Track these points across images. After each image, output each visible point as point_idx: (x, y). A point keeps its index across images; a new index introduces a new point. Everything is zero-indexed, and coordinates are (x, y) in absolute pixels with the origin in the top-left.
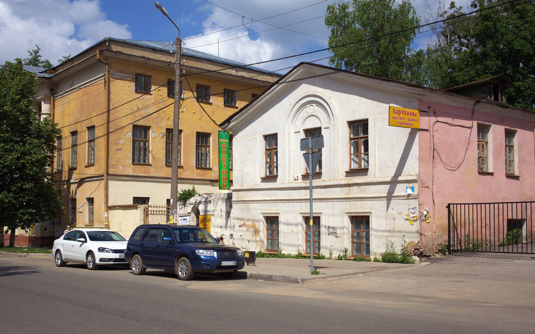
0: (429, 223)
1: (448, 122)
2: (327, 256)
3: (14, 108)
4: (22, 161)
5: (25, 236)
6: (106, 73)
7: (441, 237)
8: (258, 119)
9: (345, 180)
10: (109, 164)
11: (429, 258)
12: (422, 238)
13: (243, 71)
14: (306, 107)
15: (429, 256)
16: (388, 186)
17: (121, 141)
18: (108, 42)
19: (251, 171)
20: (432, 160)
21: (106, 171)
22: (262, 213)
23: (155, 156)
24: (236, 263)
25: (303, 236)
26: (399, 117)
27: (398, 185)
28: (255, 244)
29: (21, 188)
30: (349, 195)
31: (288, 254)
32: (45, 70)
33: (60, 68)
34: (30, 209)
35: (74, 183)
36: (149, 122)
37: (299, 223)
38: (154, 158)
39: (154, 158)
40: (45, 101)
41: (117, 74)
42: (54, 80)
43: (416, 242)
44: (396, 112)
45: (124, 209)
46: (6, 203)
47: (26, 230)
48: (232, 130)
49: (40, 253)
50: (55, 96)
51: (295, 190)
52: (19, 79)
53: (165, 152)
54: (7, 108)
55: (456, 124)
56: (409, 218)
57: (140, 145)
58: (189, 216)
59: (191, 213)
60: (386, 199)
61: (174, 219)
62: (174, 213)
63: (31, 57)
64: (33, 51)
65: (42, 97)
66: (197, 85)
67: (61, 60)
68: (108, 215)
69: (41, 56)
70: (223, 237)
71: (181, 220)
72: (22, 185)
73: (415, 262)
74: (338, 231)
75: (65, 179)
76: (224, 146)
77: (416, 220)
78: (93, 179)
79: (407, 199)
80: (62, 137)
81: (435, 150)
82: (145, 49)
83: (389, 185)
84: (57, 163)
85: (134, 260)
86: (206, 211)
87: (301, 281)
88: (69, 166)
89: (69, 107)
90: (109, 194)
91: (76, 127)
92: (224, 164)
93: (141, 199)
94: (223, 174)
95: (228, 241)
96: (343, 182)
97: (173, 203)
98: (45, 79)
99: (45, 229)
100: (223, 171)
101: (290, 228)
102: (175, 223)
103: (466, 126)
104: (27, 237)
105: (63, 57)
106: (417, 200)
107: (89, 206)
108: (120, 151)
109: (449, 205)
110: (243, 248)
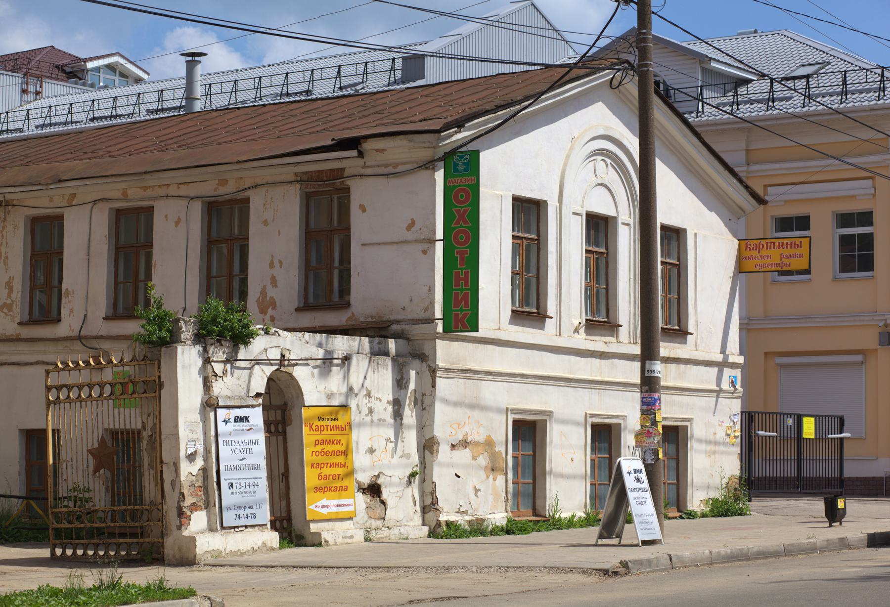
70: (379, 482)
94: (457, 285)
95: (399, 494)
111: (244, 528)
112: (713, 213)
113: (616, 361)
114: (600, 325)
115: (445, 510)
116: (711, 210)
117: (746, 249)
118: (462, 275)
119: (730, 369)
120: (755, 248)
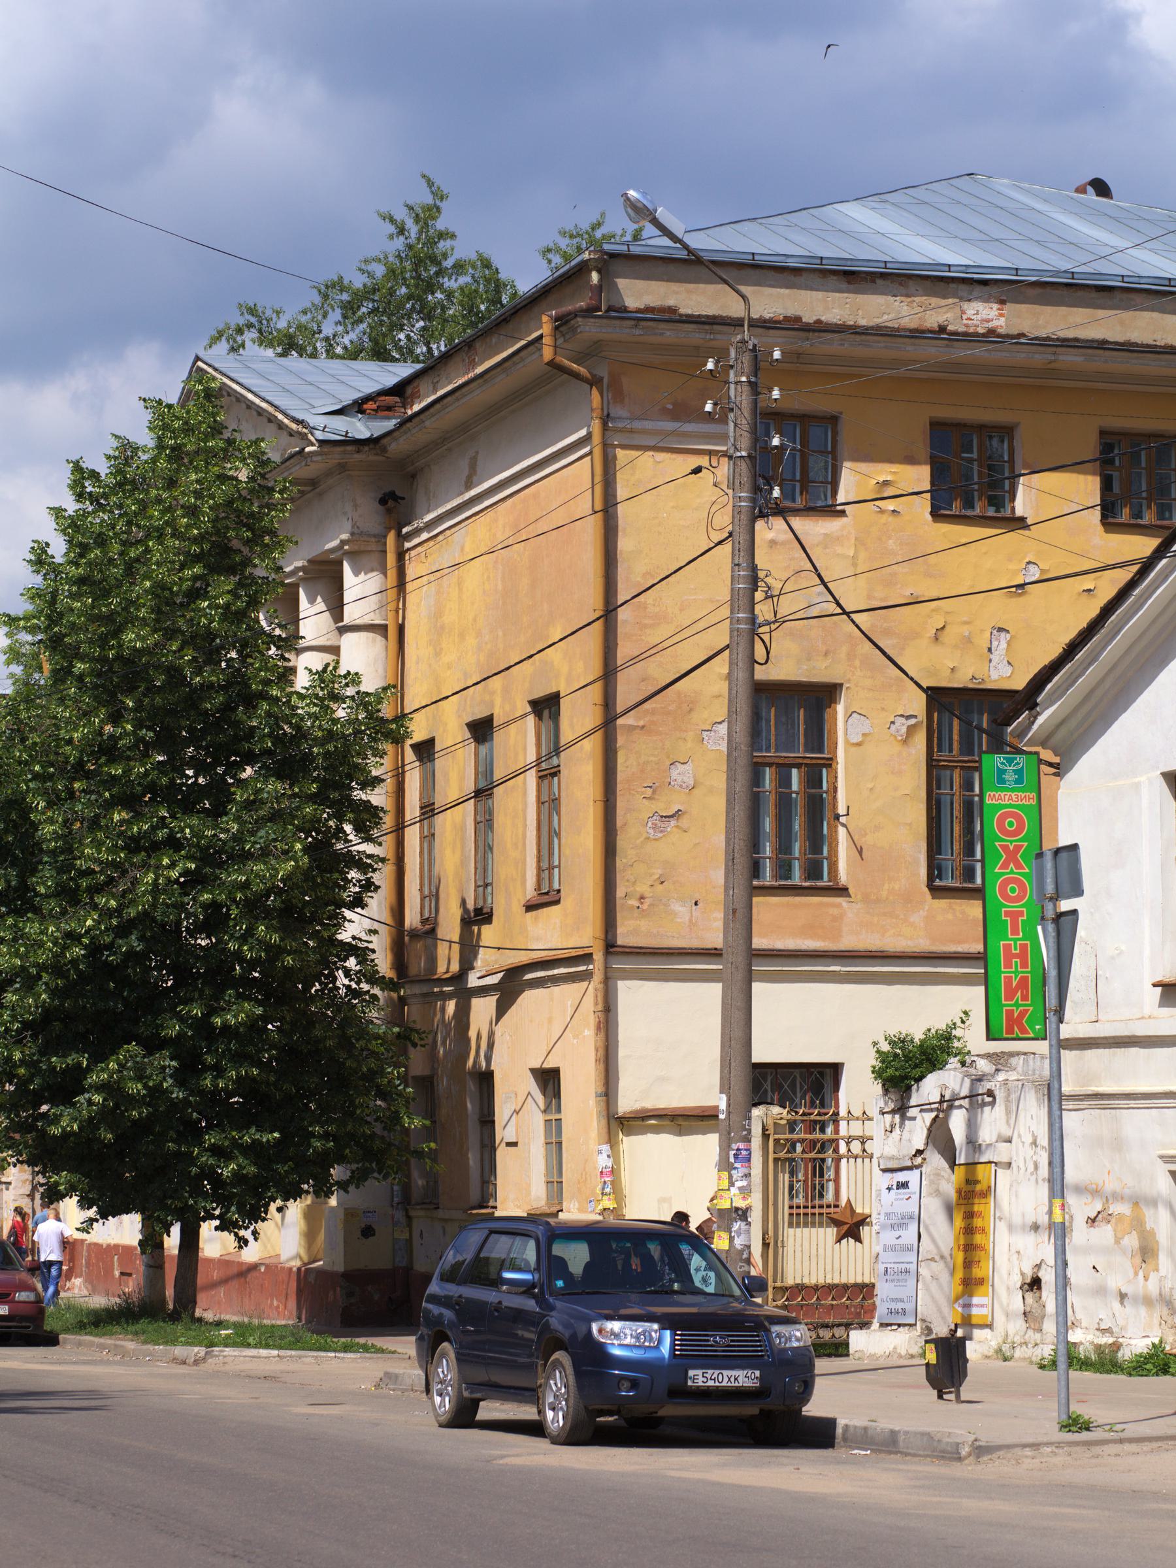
3: (171, 634)
4: (207, 896)
5: (283, 1268)
6: (596, 426)
8: (1142, 692)
10: (620, 892)
17: (682, 774)
18: (599, 271)
19: (1123, 948)
21: (600, 933)
23: (867, 841)
24: (761, 1379)
28: (1143, 1311)
29: (203, 1026)
32: (355, 402)
33: (424, 385)
34: (253, 1130)
35: (483, 991)
36: (829, 661)
38: (860, 852)
39: (860, 852)
40: (353, 555)
41: (648, 425)
42: (396, 448)
45: (680, 1132)
46: (132, 1101)
47: (242, 1233)
49: (267, 1346)
50: (405, 530)
52: (198, 481)
54: (138, 635)
57: (788, 784)
58: (917, 1167)
59: (926, 1155)
61: (734, 1190)
62: (732, 1160)
63: (399, 243)
64: (411, 208)
65: (343, 542)
66: (1103, 433)
67: (558, 250)
68: (617, 1161)
69: (453, 236)
71: (889, 1189)
72: (211, 1012)
75: (447, 972)
76: (1011, 824)
78: (556, 972)
80: (437, 748)
82: (801, 280)
84: (422, 885)
85: (437, 1367)
86: (972, 1142)
87: (970, 1454)
88: (464, 902)
89: (460, 590)
90: (622, 1052)
91: (487, 698)
93: (797, 1073)
94: (1008, 965)
97: (729, 1113)
98: (349, 448)
99: (368, 1232)
100: (1007, 948)
102: (737, 1209)
104: (290, 1269)
105: (563, 233)
107: (545, 1111)
108: (673, 822)
110: (1104, 1331)
111: (896, 1327)
115: (1084, 1325)
118: (1016, 949)
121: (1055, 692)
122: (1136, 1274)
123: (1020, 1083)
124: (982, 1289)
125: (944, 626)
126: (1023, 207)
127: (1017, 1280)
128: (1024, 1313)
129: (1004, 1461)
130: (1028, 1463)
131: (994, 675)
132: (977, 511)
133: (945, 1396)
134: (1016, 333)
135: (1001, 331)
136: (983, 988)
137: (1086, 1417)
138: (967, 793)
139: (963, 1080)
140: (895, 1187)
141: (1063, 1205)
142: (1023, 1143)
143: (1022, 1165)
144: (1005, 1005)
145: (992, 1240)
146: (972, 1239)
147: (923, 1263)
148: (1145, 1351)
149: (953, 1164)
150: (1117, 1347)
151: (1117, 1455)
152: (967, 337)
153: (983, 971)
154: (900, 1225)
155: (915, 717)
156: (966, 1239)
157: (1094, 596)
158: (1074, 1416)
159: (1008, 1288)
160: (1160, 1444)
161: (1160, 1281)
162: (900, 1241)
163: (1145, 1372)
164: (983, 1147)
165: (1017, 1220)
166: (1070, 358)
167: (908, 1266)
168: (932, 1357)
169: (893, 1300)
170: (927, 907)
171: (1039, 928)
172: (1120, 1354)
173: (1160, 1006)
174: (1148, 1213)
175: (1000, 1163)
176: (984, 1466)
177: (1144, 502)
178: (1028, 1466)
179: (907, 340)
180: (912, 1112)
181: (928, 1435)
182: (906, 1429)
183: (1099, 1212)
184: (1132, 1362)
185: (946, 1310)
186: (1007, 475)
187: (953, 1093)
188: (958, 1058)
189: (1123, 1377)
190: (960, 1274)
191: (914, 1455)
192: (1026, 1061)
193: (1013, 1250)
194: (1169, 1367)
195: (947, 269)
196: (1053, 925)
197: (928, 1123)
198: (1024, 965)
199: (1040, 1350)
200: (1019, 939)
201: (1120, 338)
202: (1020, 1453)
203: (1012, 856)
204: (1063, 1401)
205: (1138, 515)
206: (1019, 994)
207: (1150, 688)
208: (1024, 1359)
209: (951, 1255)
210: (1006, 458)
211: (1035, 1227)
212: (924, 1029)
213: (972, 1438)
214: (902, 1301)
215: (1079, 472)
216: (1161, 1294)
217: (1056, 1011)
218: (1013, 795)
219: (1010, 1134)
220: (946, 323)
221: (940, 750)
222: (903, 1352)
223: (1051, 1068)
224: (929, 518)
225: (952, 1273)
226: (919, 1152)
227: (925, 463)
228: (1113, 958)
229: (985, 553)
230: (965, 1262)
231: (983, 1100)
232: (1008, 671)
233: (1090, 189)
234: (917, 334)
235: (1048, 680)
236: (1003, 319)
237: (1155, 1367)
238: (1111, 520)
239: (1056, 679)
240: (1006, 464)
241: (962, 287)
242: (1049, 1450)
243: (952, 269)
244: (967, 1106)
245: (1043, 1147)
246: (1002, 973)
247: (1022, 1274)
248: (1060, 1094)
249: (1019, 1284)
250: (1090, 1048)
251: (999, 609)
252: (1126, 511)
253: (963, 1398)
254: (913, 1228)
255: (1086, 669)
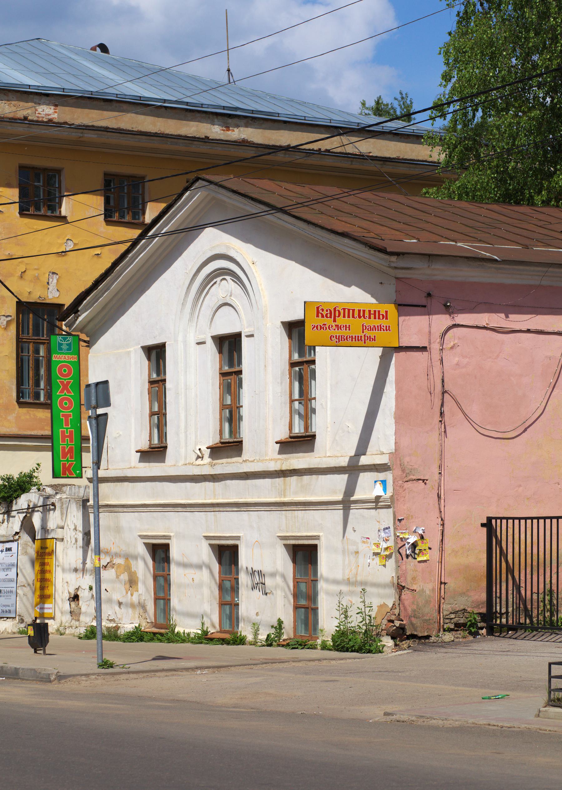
0: (425, 561)
1: (491, 325)
2: (250, 638)
7: (463, 594)
9: (276, 460)
11: (427, 641)
12: (403, 597)
13: (246, 126)
14: (215, 283)
15: (428, 637)
16: (345, 477)
19: (121, 433)
20: (437, 418)
22: (142, 537)
25: (212, 592)
26: (333, 324)
27: (362, 475)
28: (130, 611)
30: (285, 496)
31: (184, 633)
37: (203, 563)
43: (390, 606)
44: (324, 313)
48: (86, 330)
51: (196, 483)
53: (14, 368)
55: (517, 327)
56: (379, 551)
59: (21, 534)
60: (341, 506)
66: (106, 174)
71: (2, 551)
73: (385, 649)
74: (269, 581)
76: (65, 371)
77: (389, 557)
79: (376, 508)
81: (446, 395)
83: (347, 476)
86: (44, 528)
87: (55, 679)
92: (66, 417)
94: (63, 441)
96: (273, 467)
100: (63, 432)
101: (191, 573)
103: (550, 330)
106: (391, 510)
109: (489, 519)
110: (111, 621)
111: (6, 619)
112: (353, 287)
113: (228, 482)
114: (300, 441)
116: (349, 286)
117: (318, 316)
118: (67, 433)
119: (376, 473)
120: (329, 315)
121: (87, 305)
122: (127, 593)
123: (68, 500)
124: (49, 600)
125: (25, 271)
126: (66, 57)
127: (67, 596)
128: (70, 612)
129: (72, 682)
130: (84, 683)
131: (50, 296)
132: (42, 212)
133: (38, 652)
134: (63, 122)
135: (55, 120)
136: (51, 453)
137: (111, 661)
138: (37, 355)
139: (39, 498)
140: (5, 550)
141: (99, 558)
142: (70, 529)
143: (69, 540)
144: (62, 461)
145: (54, 576)
146: (44, 576)
147: (19, 588)
148: (132, 630)
149: (34, 539)
150: (117, 628)
151: (127, 679)
152: (38, 123)
153: (51, 444)
154: (7, 569)
155: (11, 316)
156: (41, 576)
157: (100, 257)
158: (105, 661)
159: (62, 600)
160: (147, 674)
161: (139, 596)
162: (7, 577)
163: (132, 640)
164: (50, 531)
165: (67, 566)
166: (90, 136)
167: (12, 589)
168: (31, 632)
169: (4, 606)
170: (16, 412)
171: (88, 422)
172: (119, 632)
173: (139, 462)
174: (133, 562)
175: (58, 538)
176: (62, 685)
177: (126, 210)
178: (84, 685)
179: (8, 123)
180: (13, 514)
181: (34, 670)
182: (23, 667)
183: (108, 563)
184: (125, 635)
185: (31, 610)
186: (57, 196)
187: (34, 504)
188: (36, 487)
189: (120, 643)
190: (38, 593)
191: (27, 680)
192: (70, 489)
193: (65, 581)
194: (144, 638)
195: (28, 87)
196: (95, 421)
197: (21, 519)
198: (71, 441)
199: (78, 630)
200: (69, 428)
201: (115, 126)
202: (80, 679)
203: (65, 387)
204: (100, 654)
205: (123, 217)
206: (69, 455)
207: (136, 304)
208: (71, 634)
209: (33, 584)
210: (57, 186)
211: (76, 570)
212: (19, 473)
213: (56, 671)
214: (9, 606)
215: (94, 195)
216: (139, 603)
217: (96, 463)
218: (66, 356)
219: (63, 524)
220: (27, 115)
221: (23, 333)
222: (10, 631)
223: (94, 491)
224: (18, 215)
225: (34, 593)
226: (17, 533)
227: (16, 187)
228: (116, 438)
229: (46, 234)
230: (40, 587)
231: (49, 508)
232: (57, 294)
233: (98, 49)
234: (13, 120)
235: (84, 299)
236: (56, 114)
237: (136, 638)
238: (109, 219)
239: (88, 298)
240: (57, 189)
241: (36, 97)
242: (94, 677)
243: (31, 87)
244: (41, 511)
245: (80, 531)
246: (60, 445)
247: (69, 593)
248: (99, 506)
249: (68, 598)
250: (104, 482)
251: (53, 263)
252: (117, 215)
253: (47, 653)
254: (14, 570)
255: (104, 294)
